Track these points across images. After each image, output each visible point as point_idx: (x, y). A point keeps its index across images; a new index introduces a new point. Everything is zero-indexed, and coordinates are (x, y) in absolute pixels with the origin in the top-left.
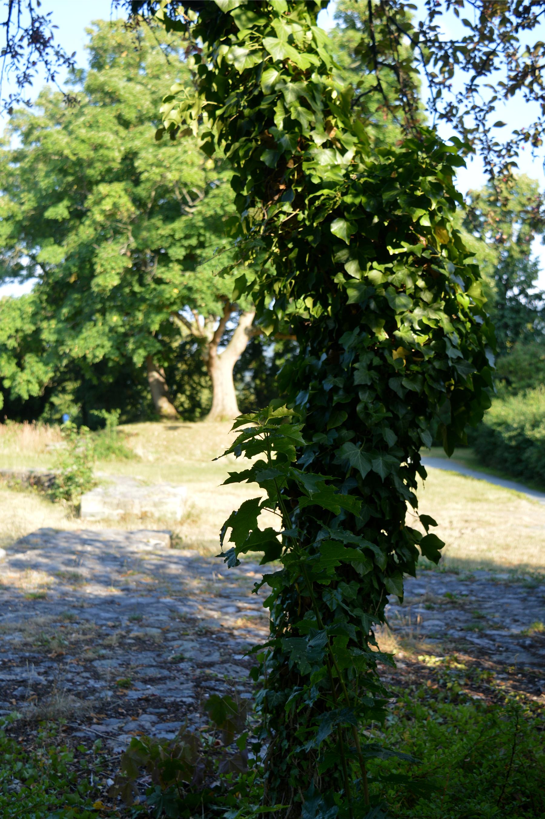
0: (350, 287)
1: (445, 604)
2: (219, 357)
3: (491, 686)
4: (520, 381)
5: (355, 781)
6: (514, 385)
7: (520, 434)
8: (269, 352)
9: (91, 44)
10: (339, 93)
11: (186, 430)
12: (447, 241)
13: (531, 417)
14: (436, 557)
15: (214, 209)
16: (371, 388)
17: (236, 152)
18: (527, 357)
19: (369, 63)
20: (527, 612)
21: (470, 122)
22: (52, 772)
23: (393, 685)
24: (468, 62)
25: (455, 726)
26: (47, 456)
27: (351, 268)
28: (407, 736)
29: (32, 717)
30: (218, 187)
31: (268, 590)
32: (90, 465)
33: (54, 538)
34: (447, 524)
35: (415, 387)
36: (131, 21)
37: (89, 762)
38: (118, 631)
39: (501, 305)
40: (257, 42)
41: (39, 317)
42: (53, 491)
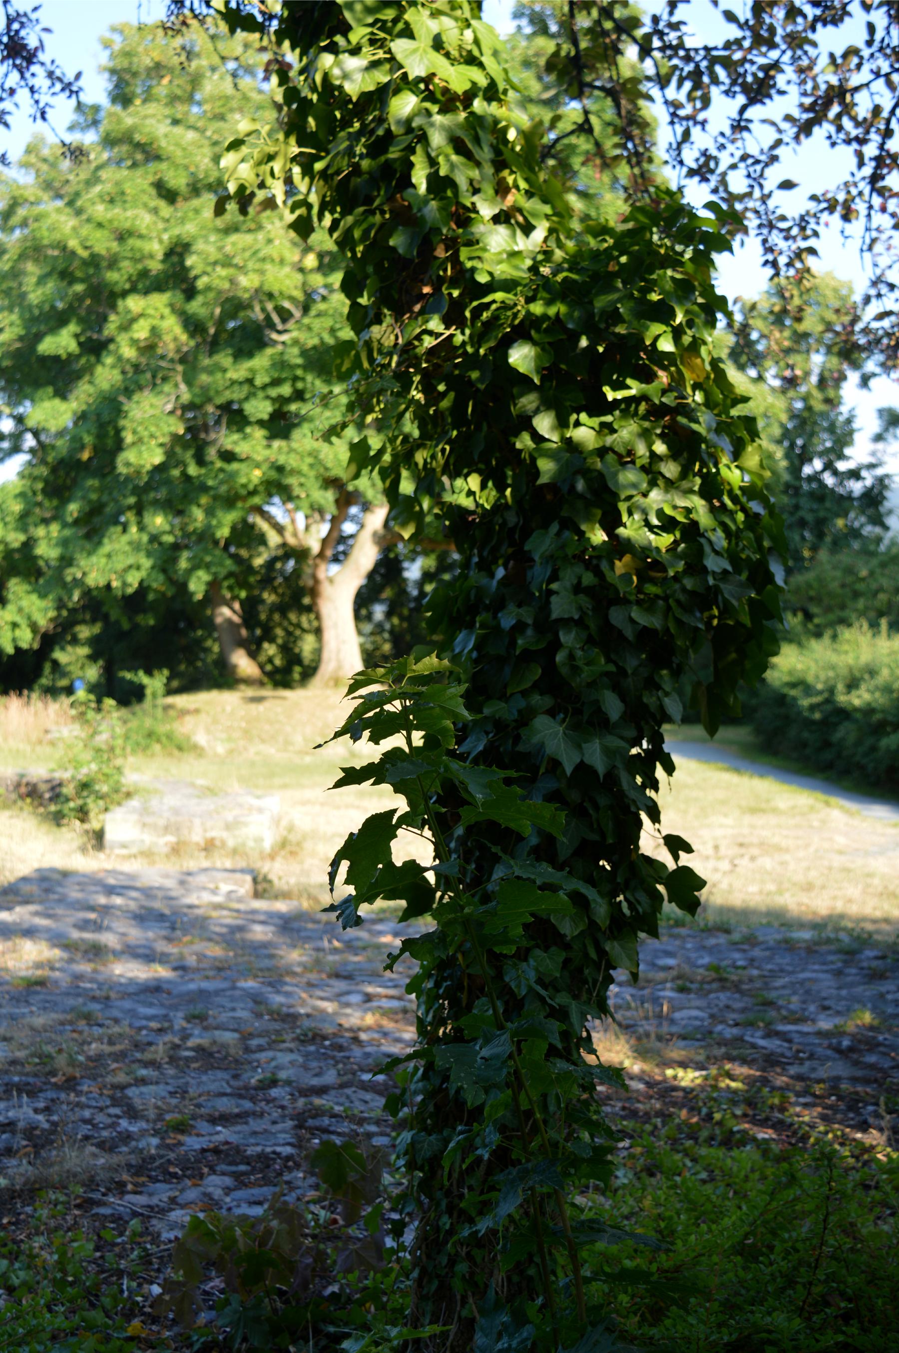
0: (541, 455)
1: (709, 983)
2: (331, 580)
3: (786, 1117)
4: (826, 614)
5: (562, 1281)
6: (816, 621)
7: (829, 701)
8: (413, 571)
9: (111, 64)
10: (520, 132)
11: (278, 702)
12: (703, 375)
13: (844, 672)
14: (692, 905)
15: (319, 335)
16: (580, 623)
17: (348, 232)
18: (838, 574)
19: (570, 85)
20: (844, 992)
21: (738, 183)
22: (59, 1275)
23: (624, 1118)
24: (734, 83)
25: (728, 1185)
26: (48, 750)
27: (544, 424)
28: (647, 1202)
29: (25, 1184)
30: (324, 298)
31: (411, 966)
32: (118, 762)
33: (60, 884)
34: (710, 851)
35: (653, 621)
36: (173, 18)
37: (120, 1256)
38: (168, 1038)
39: (793, 489)
40: (381, 47)
41: (30, 520)
42: (58, 807)
